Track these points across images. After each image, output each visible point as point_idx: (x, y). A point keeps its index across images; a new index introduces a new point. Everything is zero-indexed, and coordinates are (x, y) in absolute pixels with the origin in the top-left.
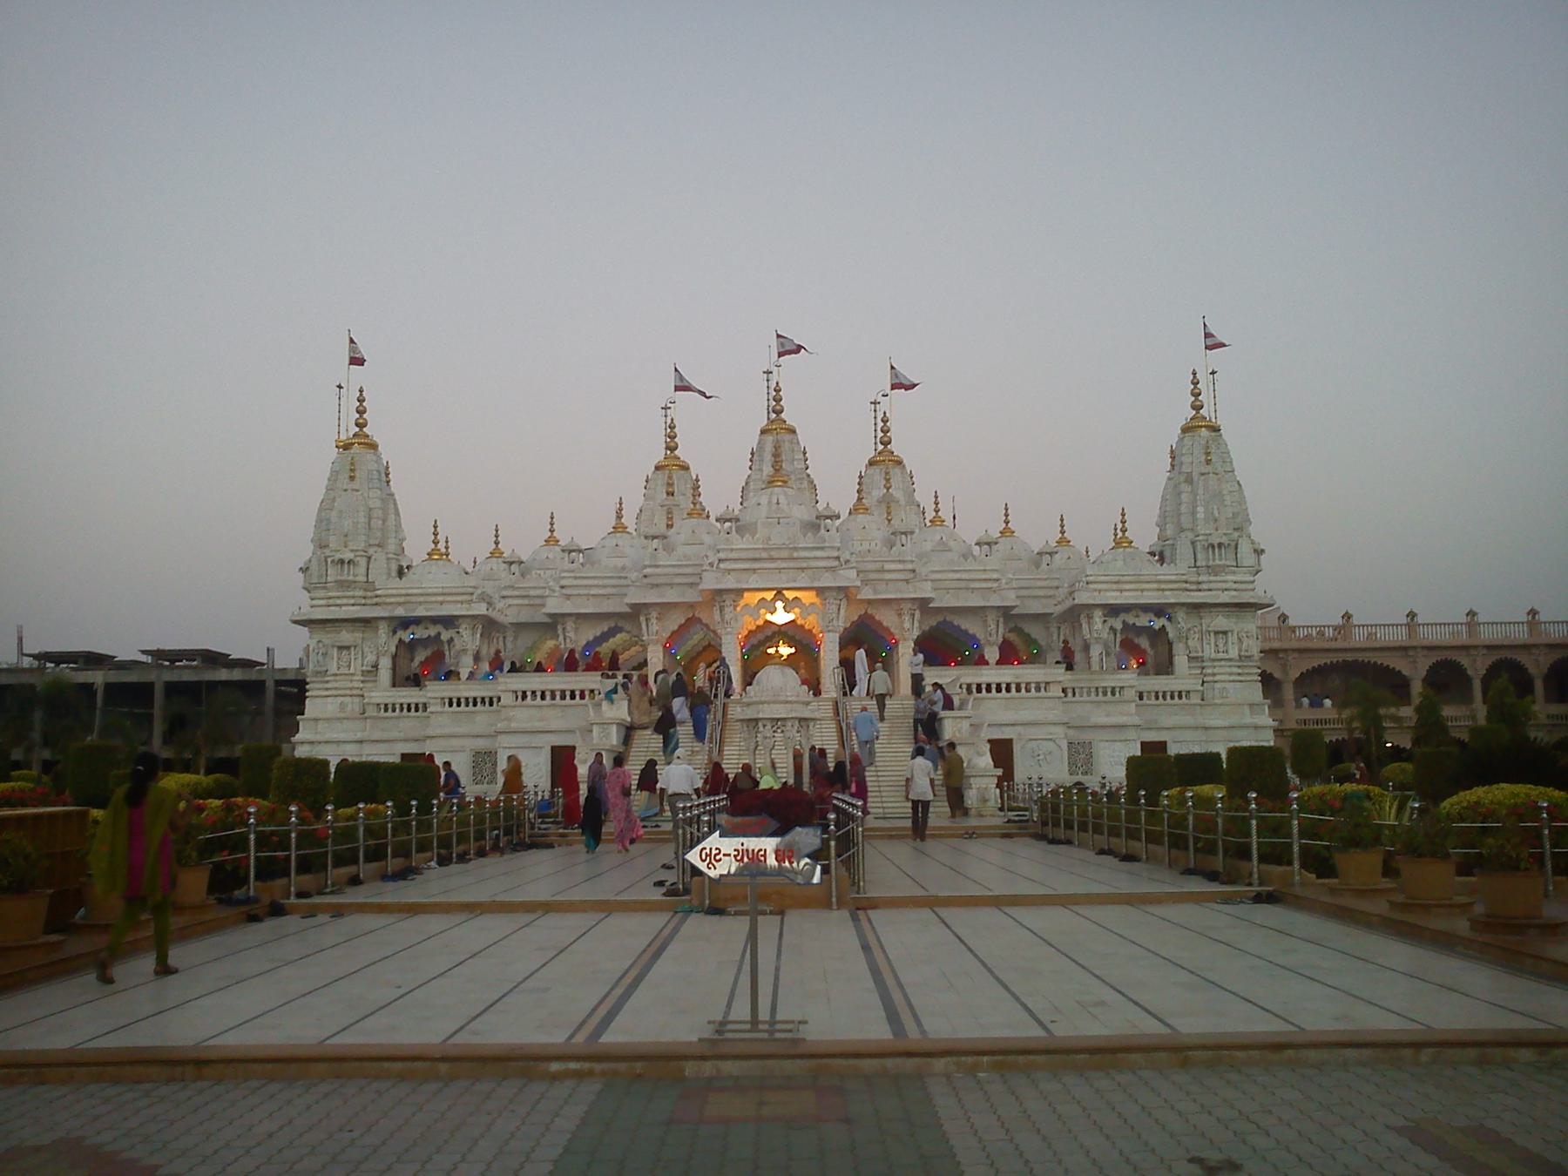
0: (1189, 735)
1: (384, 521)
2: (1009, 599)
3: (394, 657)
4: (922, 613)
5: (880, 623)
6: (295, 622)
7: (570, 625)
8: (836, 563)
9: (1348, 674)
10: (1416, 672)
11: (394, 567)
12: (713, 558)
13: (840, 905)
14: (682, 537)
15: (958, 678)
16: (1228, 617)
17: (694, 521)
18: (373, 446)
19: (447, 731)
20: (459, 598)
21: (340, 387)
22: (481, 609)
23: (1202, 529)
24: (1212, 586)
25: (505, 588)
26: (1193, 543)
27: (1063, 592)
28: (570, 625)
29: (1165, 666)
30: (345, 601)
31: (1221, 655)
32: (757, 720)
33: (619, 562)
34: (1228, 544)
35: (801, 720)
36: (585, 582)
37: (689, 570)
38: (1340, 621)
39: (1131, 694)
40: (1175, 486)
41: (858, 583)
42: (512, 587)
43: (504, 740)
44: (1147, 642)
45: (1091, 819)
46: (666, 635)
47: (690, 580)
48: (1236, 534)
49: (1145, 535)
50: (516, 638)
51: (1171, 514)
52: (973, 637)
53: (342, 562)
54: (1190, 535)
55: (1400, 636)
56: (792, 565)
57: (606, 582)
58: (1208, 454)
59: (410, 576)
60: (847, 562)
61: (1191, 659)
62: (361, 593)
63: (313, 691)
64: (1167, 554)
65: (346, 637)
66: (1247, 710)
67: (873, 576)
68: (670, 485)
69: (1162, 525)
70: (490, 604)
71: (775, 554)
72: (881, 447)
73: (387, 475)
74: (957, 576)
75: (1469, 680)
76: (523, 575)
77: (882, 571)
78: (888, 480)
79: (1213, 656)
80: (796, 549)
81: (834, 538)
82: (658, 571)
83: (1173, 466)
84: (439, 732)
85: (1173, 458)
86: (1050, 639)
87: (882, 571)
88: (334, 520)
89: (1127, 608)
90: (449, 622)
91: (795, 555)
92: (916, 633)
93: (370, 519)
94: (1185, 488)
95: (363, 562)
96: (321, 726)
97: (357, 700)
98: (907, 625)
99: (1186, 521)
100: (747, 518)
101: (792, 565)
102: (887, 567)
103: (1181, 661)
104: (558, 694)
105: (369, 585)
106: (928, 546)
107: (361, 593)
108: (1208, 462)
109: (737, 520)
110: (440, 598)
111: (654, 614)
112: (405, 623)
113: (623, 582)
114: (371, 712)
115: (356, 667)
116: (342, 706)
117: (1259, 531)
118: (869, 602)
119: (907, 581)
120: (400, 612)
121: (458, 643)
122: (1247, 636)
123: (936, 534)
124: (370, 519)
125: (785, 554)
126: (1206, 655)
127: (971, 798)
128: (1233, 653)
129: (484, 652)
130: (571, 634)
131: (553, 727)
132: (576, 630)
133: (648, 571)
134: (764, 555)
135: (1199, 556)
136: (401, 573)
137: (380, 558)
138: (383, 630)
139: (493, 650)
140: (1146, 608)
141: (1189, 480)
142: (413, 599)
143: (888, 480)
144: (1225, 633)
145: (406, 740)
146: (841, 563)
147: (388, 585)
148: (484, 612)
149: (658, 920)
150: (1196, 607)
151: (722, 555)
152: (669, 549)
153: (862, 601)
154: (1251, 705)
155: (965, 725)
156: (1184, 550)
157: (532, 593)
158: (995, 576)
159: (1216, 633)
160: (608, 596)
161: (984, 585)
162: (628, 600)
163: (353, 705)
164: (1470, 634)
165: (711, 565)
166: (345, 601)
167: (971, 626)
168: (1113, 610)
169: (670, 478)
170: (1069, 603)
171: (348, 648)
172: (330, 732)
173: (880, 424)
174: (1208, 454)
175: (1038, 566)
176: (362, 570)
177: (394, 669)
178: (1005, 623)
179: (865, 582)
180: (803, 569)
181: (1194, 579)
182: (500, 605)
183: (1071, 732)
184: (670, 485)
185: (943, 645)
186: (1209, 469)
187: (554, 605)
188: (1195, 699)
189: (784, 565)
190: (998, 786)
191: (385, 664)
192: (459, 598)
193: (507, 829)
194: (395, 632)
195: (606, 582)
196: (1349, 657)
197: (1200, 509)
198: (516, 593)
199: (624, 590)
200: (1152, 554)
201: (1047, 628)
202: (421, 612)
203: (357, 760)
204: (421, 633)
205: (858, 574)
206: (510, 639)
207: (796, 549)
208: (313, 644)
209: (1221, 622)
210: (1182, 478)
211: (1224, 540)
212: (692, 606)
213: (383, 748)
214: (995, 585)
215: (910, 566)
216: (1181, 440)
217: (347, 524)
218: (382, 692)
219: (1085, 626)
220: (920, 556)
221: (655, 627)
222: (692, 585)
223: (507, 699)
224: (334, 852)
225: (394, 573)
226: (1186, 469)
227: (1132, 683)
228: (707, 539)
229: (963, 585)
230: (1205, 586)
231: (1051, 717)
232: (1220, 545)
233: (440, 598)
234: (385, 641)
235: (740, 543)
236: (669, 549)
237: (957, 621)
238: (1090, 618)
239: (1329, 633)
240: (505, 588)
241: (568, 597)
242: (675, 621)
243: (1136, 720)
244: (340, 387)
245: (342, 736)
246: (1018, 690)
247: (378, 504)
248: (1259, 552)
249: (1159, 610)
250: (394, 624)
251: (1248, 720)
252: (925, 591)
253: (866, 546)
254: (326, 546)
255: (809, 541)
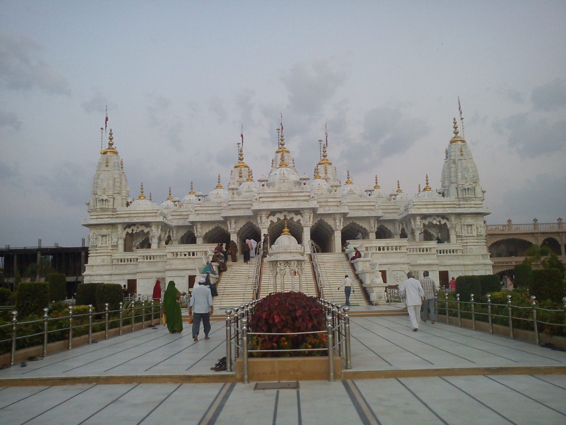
0: (458, 268)
1: (121, 183)
2: (379, 213)
3: (125, 240)
4: (344, 220)
5: (327, 223)
6: (84, 225)
7: (199, 226)
8: (308, 198)
9: (505, 245)
10: (538, 242)
11: (125, 202)
12: (257, 196)
13: (336, 377)
14: (244, 189)
15: (362, 244)
16: (472, 219)
17: (249, 183)
18: (116, 153)
19: (145, 270)
20: (151, 215)
21: (102, 129)
22: (160, 219)
23: (461, 182)
24: (465, 206)
25: (173, 212)
26: (457, 188)
27: (402, 209)
28: (199, 226)
29: (448, 239)
30: (104, 216)
31: (470, 235)
32: (277, 261)
33: (219, 200)
34: (467, 192)
35: (298, 261)
36: (205, 208)
37: (247, 203)
38: (506, 223)
39: (434, 251)
40: (448, 165)
41: (318, 206)
42: (175, 211)
43: (168, 274)
44: (437, 230)
45: (447, 309)
46: (238, 229)
47: (248, 206)
48: (474, 184)
49: (436, 184)
50: (177, 232)
51: (448, 177)
52: (365, 229)
53: (103, 200)
54: (455, 185)
55: (531, 229)
56: (290, 199)
57: (213, 208)
58: (462, 151)
59: (131, 206)
60: (313, 197)
61: (457, 236)
62: (111, 213)
63: (92, 254)
64: (446, 193)
65: (104, 231)
66: (481, 257)
67: (323, 204)
68: (241, 173)
69: (443, 183)
70: (165, 217)
71: (283, 195)
72: (323, 158)
73: (122, 165)
74: (357, 204)
75: (559, 246)
76: (180, 206)
77: (327, 202)
78: (326, 170)
79: (466, 235)
80: (292, 192)
81: (307, 187)
82: (235, 203)
83: (447, 157)
84: (142, 270)
85: (447, 154)
86: (396, 229)
87: (327, 202)
88: (99, 183)
89: (430, 216)
90: (147, 224)
91: (291, 195)
92: (342, 227)
93: (114, 182)
94: (453, 165)
95: (112, 200)
96: (95, 268)
97: (109, 257)
98: (338, 224)
99: (453, 179)
100: (271, 180)
101: (290, 199)
102: (330, 200)
103: (453, 237)
104: (191, 253)
105: (114, 210)
106: (345, 192)
107: (111, 213)
108: (462, 155)
109: (267, 181)
110: (143, 215)
111: (233, 221)
112: (129, 225)
113: (220, 208)
114: (115, 262)
115: (109, 244)
116: (103, 260)
117: (483, 184)
118: (322, 214)
119: (337, 206)
120: (127, 220)
121: (151, 234)
122: (479, 227)
123: (349, 187)
124: (114, 182)
125: (287, 195)
126: (463, 235)
127: (374, 297)
128: (475, 234)
129: (163, 237)
130: (199, 230)
131: (189, 268)
132: (201, 228)
133: (230, 203)
134: (278, 195)
135: (460, 193)
136: (128, 204)
137: (118, 198)
138: (120, 228)
139: (167, 236)
140: (438, 215)
141: (454, 162)
142: (132, 215)
143: (326, 170)
144: (471, 225)
145: (130, 274)
146: (310, 198)
147: (121, 209)
148: (162, 220)
149: (211, 391)
150: (459, 215)
151: (261, 195)
152: (239, 194)
153: (319, 214)
154: (483, 255)
155: (368, 264)
156: (453, 190)
157: (184, 213)
158: (373, 204)
159: (468, 225)
160: (214, 214)
161: (369, 208)
162: (222, 215)
163: (107, 260)
164: (559, 228)
165: (256, 199)
166: (104, 216)
167: (364, 225)
168: (424, 217)
169: (241, 170)
170: (405, 214)
171: (105, 236)
172: (96, 272)
173: (322, 149)
174: (462, 151)
175: (390, 200)
176: (111, 203)
177: (125, 245)
178: (378, 223)
179: (321, 206)
180: (294, 201)
181: (458, 203)
182: (170, 218)
183: (410, 267)
184: (241, 173)
185: (350, 234)
186: (462, 158)
187: (192, 218)
188: (459, 253)
189: (287, 199)
190: (386, 291)
191: (121, 242)
192: (151, 215)
193: (146, 316)
194: (125, 229)
195: (213, 208)
196: (511, 237)
197: (459, 174)
198: (177, 214)
199: (221, 212)
200: (440, 193)
201: (394, 225)
202: (135, 220)
203: (109, 283)
204: (136, 230)
205: (318, 203)
206: (175, 232)
207: (292, 192)
208: (91, 234)
209: (469, 221)
210: (451, 161)
211: (470, 187)
212: (249, 217)
213: (119, 277)
214: (374, 207)
215: (339, 200)
216: (450, 146)
217: (105, 185)
218: (120, 253)
219: (413, 223)
220: (343, 196)
221: (233, 226)
222: (248, 208)
223: (170, 256)
224: (17, 341)
225: (125, 205)
226: (453, 158)
227: (436, 246)
228: (254, 189)
229: (360, 208)
230: (462, 206)
231: (402, 261)
232: (468, 189)
233: (143, 215)
234: (121, 233)
235: (268, 190)
236: (239, 194)
237: (358, 223)
238: (415, 220)
239: (501, 228)
240: (173, 212)
241: (198, 214)
242: (241, 224)
243: (436, 262)
244: (102, 129)
245: (103, 273)
246: (388, 249)
247: (118, 176)
248: (484, 192)
249: (443, 216)
250: (125, 225)
251: (482, 261)
252: (345, 210)
253: (320, 192)
254: (96, 194)
255: (297, 189)
